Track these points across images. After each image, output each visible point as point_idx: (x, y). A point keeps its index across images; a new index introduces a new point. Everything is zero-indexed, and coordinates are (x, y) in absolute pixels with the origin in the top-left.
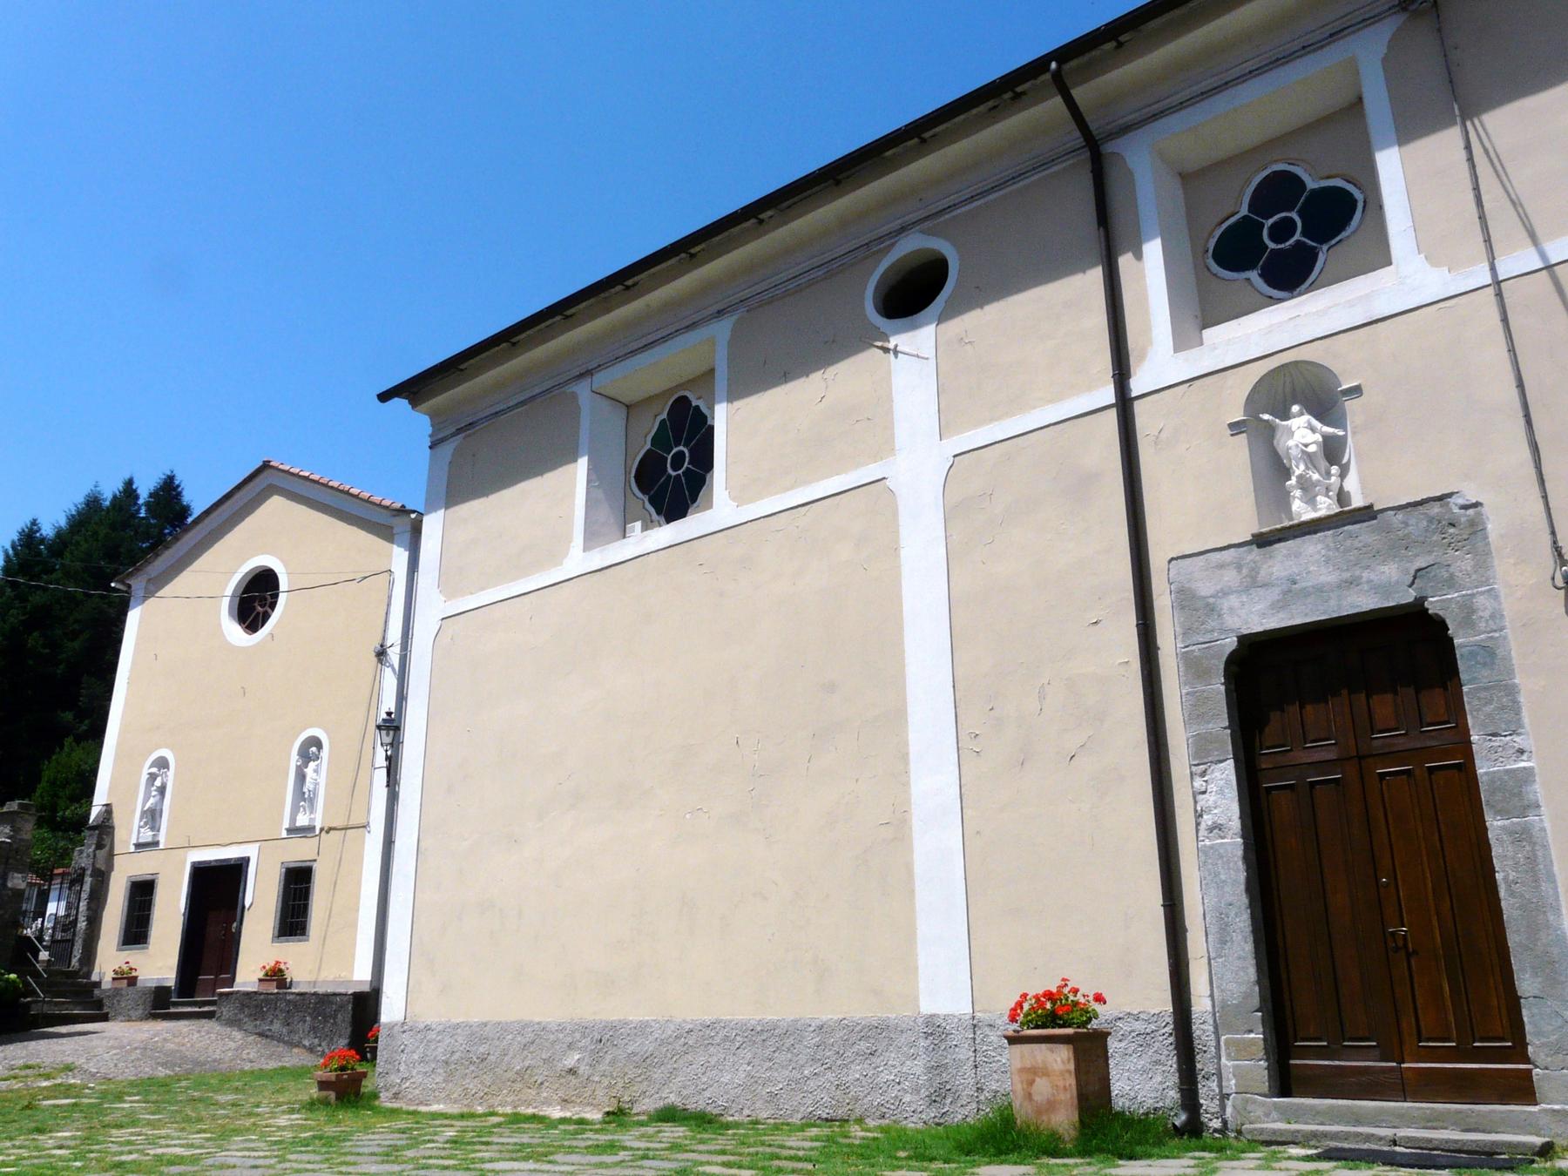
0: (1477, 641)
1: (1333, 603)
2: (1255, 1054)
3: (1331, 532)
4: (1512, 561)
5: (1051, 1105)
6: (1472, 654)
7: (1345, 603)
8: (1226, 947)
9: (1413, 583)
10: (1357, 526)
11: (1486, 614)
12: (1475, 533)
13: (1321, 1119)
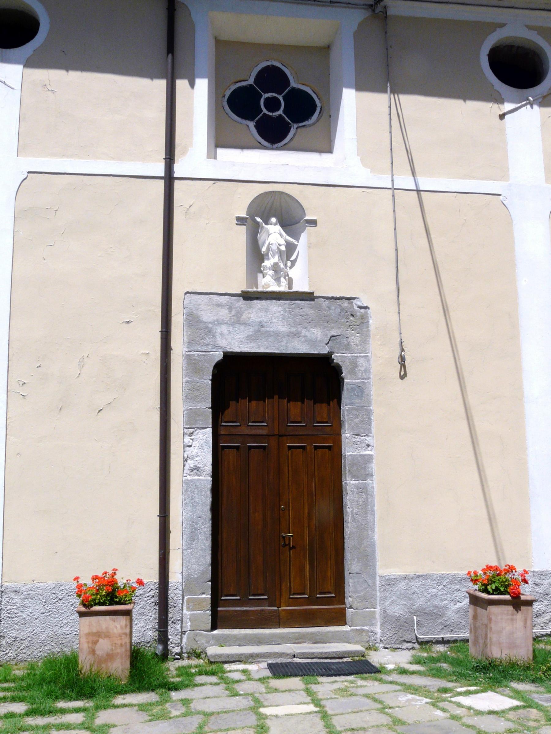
0: (356, 382)
1: (283, 344)
2: (204, 607)
3: (288, 302)
4: (379, 343)
5: (110, 657)
6: (353, 389)
7: (290, 345)
8: (194, 543)
9: (328, 343)
10: (303, 302)
11: (362, 369)
12: (363, 323)
13: (239, 642)
